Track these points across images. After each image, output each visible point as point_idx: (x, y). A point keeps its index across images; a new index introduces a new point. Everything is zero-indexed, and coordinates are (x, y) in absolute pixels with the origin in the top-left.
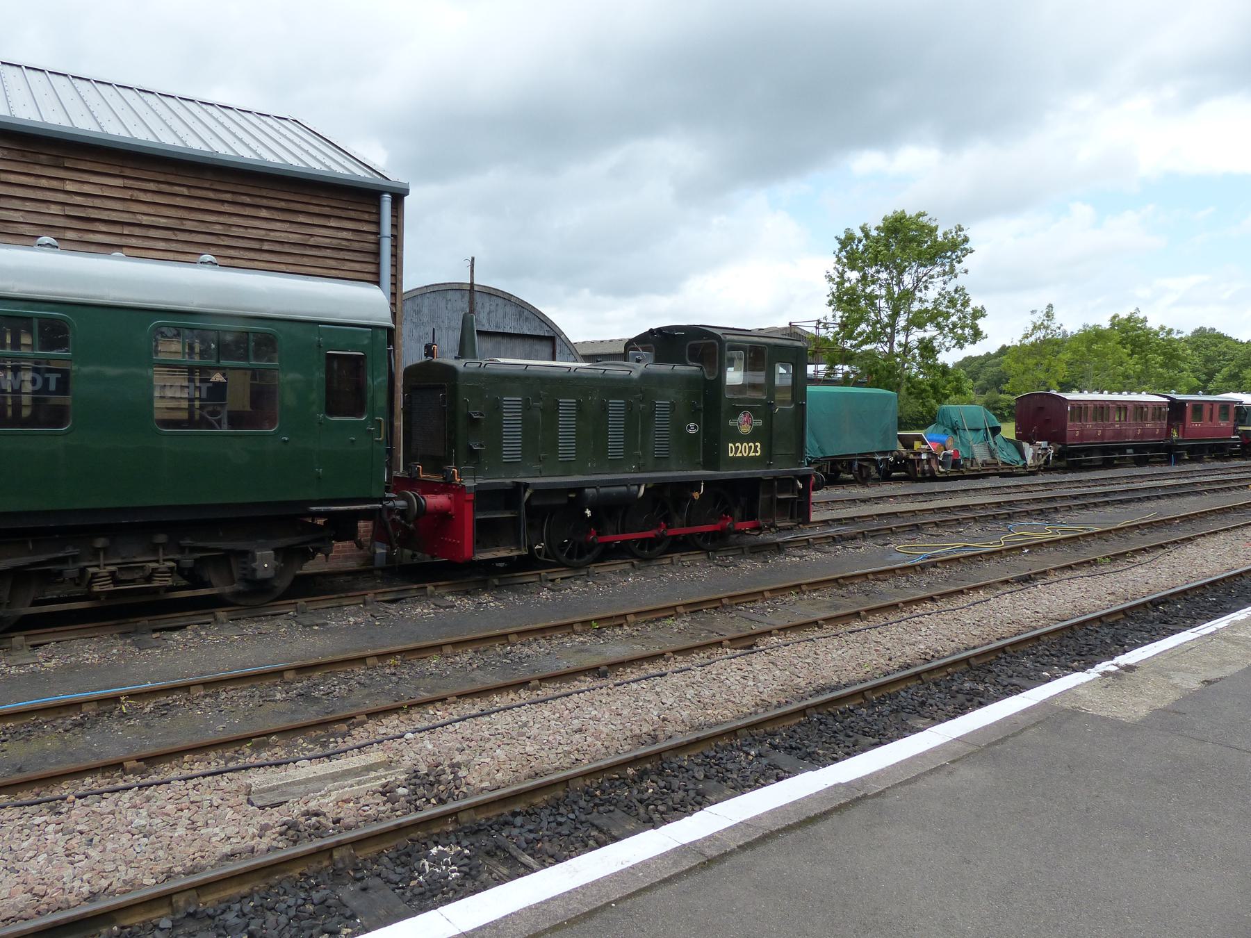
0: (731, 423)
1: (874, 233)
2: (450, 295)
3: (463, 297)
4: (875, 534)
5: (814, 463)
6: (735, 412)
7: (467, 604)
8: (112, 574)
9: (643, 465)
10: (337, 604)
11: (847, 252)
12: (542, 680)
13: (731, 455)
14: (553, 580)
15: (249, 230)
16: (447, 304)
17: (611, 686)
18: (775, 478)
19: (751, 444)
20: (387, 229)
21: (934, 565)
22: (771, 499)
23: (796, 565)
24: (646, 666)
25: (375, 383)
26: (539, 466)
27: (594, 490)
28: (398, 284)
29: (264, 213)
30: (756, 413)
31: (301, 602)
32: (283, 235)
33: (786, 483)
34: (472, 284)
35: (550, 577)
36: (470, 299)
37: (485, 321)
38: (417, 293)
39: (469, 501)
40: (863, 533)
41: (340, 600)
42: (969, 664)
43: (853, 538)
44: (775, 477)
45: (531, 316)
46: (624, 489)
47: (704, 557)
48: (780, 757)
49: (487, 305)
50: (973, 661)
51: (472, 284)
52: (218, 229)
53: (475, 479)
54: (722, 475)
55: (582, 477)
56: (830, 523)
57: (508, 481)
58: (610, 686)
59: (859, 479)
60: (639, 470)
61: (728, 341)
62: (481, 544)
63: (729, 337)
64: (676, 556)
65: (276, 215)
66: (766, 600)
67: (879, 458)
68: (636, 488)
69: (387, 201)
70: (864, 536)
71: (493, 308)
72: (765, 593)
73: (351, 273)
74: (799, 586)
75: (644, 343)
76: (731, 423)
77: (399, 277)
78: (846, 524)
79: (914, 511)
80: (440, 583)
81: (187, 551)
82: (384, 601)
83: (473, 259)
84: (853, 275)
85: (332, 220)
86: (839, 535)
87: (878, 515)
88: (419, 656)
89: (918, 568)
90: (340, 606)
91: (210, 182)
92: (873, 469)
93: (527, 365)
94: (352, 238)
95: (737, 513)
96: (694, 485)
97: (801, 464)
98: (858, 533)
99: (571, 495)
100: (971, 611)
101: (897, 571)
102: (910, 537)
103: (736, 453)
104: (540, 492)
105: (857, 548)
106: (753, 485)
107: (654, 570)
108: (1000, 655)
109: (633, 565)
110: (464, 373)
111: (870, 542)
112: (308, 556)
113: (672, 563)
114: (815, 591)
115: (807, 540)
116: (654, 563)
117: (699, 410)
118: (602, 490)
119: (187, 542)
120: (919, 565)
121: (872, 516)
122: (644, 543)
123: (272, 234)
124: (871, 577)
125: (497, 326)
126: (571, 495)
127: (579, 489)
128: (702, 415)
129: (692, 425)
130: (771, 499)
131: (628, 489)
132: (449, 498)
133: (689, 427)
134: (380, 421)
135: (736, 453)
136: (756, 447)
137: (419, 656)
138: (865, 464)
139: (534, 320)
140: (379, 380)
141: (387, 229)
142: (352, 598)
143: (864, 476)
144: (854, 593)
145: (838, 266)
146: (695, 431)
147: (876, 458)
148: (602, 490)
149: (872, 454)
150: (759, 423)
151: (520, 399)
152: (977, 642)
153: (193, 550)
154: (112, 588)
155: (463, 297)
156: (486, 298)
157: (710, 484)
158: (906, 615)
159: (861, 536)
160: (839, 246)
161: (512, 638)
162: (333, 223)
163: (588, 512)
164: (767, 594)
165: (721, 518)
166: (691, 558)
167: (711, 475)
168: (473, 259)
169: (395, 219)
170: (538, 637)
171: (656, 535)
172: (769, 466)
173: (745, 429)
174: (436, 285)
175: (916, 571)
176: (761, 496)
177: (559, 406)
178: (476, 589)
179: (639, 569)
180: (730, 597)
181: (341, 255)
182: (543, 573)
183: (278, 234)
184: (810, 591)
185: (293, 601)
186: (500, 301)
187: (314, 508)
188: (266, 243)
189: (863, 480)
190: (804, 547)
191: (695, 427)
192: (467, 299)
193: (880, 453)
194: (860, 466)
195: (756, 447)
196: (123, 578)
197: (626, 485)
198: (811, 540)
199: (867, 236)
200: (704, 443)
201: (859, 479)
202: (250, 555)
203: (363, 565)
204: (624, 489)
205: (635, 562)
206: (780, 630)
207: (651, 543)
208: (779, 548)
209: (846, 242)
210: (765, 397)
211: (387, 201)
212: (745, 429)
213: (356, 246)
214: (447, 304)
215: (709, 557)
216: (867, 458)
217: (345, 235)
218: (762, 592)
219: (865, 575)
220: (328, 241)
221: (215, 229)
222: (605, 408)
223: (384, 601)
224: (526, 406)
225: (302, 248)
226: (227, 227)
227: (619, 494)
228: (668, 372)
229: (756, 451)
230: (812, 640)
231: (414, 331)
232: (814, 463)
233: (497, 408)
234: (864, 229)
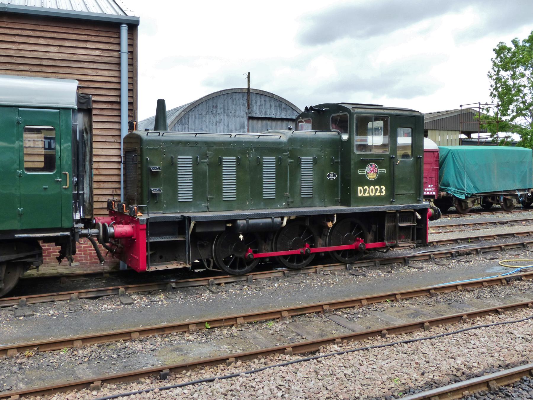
0: (360, 172)
1: (521, 44)
2: (235, 96)
3: (243, 97)
4: (488, 250)
5: (470, 197)
6: (363, 164)
7: (145, 300)
9: (292, 202)
10: (50, 300)
11: (501, 58)
12: (104, 381)
13: (360, 195)
14: (219, 284)
15: (32, 53)
16: (233, 101)
17: (156, 390)
18: (397, 211)
19: (377, 187)
20: (124, 47)
21: (519, 279)
22: (395, 226)
23: (412, 276)
25: (62, 147)
26: (207, 204)
27: (245, 222)
28: (135, 84)
29: (42, 41)
30: (379, 164)
31: (23, 298)
32: (55, 54)
33: (407, 215)
34: (249, 89)
35: (217, 282)
36: (248, 97)
38: (215, 95)
39: (143, 229)
40: (476, 250)
41: (53, 297)
42: (488, 386)
43: (468, 254)
44: (397, 211)
45: (287, 107)
46: (269, 220)
47: (343, 267)
49: (259, 101)
50: (494, 385)
51: (249, 89)
52: (12, 53)
53: (148, 214)
54: (351, 209)
55: (241, 211)
56: (459, 241)
57: (178, 215)
58: (155, 391)
59: (505, 208)
60: (288, 206)
61: (356, 113)
62: (151, 259)
63: (356, 110)
64: (320, 267)
65: (51, 42)
66: (362, 306)
67: (519, 193)
68: (279, 220)
69: (124, 29)
70: (476, 252)
72: (362, 301)
73: (102, 77)
74: (394, 295)
75: (306, 117)
76: (360, 172)
77: (135, 79)
78: (472, 242)
79: (528, 233)
80: (130, 286)
82: (87, 298)
83: (249, 73)
84: (505, 74)
85: (88, 43)
86: (456, 252)
87: (498, 236)
88: (53, 349)
89: (504, 281)
90: (53, 301)
91: (6, 23)
92: (515, 201)
93: (259, 136)
94: (102, 55)
95: (370, 237)
96: (329, 217)
97: (418, 201)
98: (472, 250)
99: (228, 225)
100: (527, 325)
101: (484, 284)
102: (516, 253)
103: (364, 193)
104: (199, 223)
105: (468, 261)
106: (380, 216)
107: (298, 278)
108: (525, 378)
109: (284, 274)
110: (146, 140)
111: (481, 257)
112: (27, 266)
113: (316, 272)
114: (407, 299)
115: (429, 255)
116: (302, 272)
117: (337, 163)
118: (251, 221)
120: (505, 279)
121: (493, 236)
122: (292, 258)
123: (48, 54)
124: (460, 288)
125: (265, 114)
126: (228, 225)
127: (233, 221)
128: (339, 166)
129: (331, 174)
130: (395, 226)
131: (247, 222)
132: (133, 227)
133: (329, 175)
134: (66, 174)
135: (364, 193)
136: (381, 189)
137: (53, 349)
138: (509, 197)
139: (289, 109)
140: (65, 145)
141: (124, 47)
142: (62, 296)
143: (508, 205)
144: (440, 302)
145: (495, 68)
146: (334, 178)
147: (517, 193)
148: (251, 221)
149: (514, 191)
150: (384, 171)
151: (191, 157)
152: (514, 359)
155: (243, 97)
156: (258, 97)
157: (342, 216)
158: (466, 326)
159: (475, 252)
160: (496, 55)
161: (135, 336)
162: (89, 45)
163: (241, 237)
164: (364, 302)
165: (356, 240)
166: (333, 268)
167: (345, 210)
168: (249, 73)
169: (131, 41)
170: (157, 334)
171: (301, 253)
172: (392, 203)
173: (372, 176)
174: (226, 90)
175: (502, 283)
176: (387, 225)
177: (300, 161)
178: (158, 290)
179: (288, 277)
180: (330, 304)
181: (95, 66)
182: (211, 279)
183: (51, 54)
184: (403, 300)
185: (17, 298)
186: (267, 99)
188: (44, 60)
189: (508, 207)
190: (427, 261)
191: (334, 175)
192: (245, 98)
193: (519, 190)
194: (505, 199)
195: (381, 189)
197: (271, 218)
198: (432, 256)
199: (516, 46)
200: (341, 186)
201: (505, 208)
203: (114, 268)
204: (269, 220)
205: (286, 272)
206: (343, 338)
207: (299, 258)
208: (405, 261)
209: (501, 50)
210: (388, 153)
211: (124, 29)
212: (372, 176)
213: (105, 60)
214: (233, 101)
215: (346, 268)
216: (510, 193)
217: (98, 53)
218: (360, 301)
219: (456, 287)
220: (86, 57)
221: (9, 53)
222: (259, 164)
223: (87, 298)
224: (196, 163)
225: (69, 62)
226: (18, 51)
227: (266, 224)
228: (311, 137)
229: (381, 192)
230: (367, 349)
231: (213, 118)
232: (470, 197)
233: (172, 165)
234: (515, 42)
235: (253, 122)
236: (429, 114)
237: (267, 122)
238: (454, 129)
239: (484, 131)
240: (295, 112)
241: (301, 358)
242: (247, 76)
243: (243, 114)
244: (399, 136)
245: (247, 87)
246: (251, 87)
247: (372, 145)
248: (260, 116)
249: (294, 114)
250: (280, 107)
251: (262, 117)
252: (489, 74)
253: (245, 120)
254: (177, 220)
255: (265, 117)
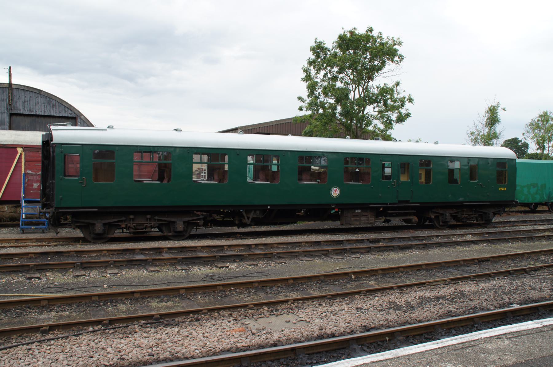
8: (134, 226)
24: (509, 262)
34: (10, 84)
37: (21, 107)
48: (337, 360)
56: (412, 238)
71: (27, 99)
81: (156, 220)
83: (10, 68)
119: (156, 218)
125: (30, 111)
153: (158, 220)
154: (134, 231)
156: (22, 93)
168: (10, 68)
186: (32, 95)
187: (61, 210)
192: (6, 93)
196: (138, 228)
202: (444, 215)
237: (34, 118)
239: (281, 133)
240: (67, 110)
241: (154, 321)
245: (7, 82)
248: (25, 113)
249: (66, 111)
250: (49, 104)
254: (380, 218)
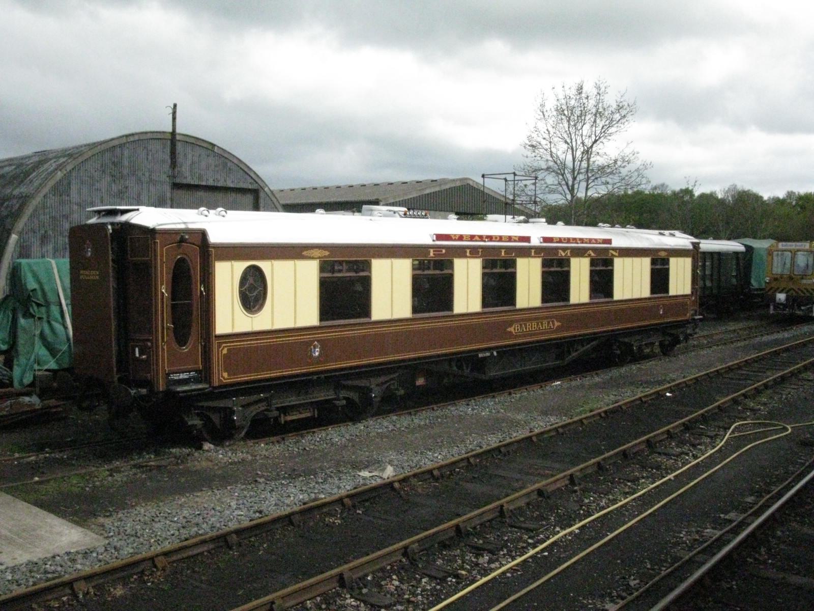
34: (173, 133)
51: (173, 133)
83: (175, 106)
168: (175, 106)
235: (180, 193)
236: (432, 181)
238: (446, 210)
242: (171, 111)
243: (164, 177)
244: (264, 207)
245: (170, 130)
246: (178, 131)
247: (783, 339)
251: (196, 183)
252: (598, 83)
253: (167, 189)
255: (200, 183)
